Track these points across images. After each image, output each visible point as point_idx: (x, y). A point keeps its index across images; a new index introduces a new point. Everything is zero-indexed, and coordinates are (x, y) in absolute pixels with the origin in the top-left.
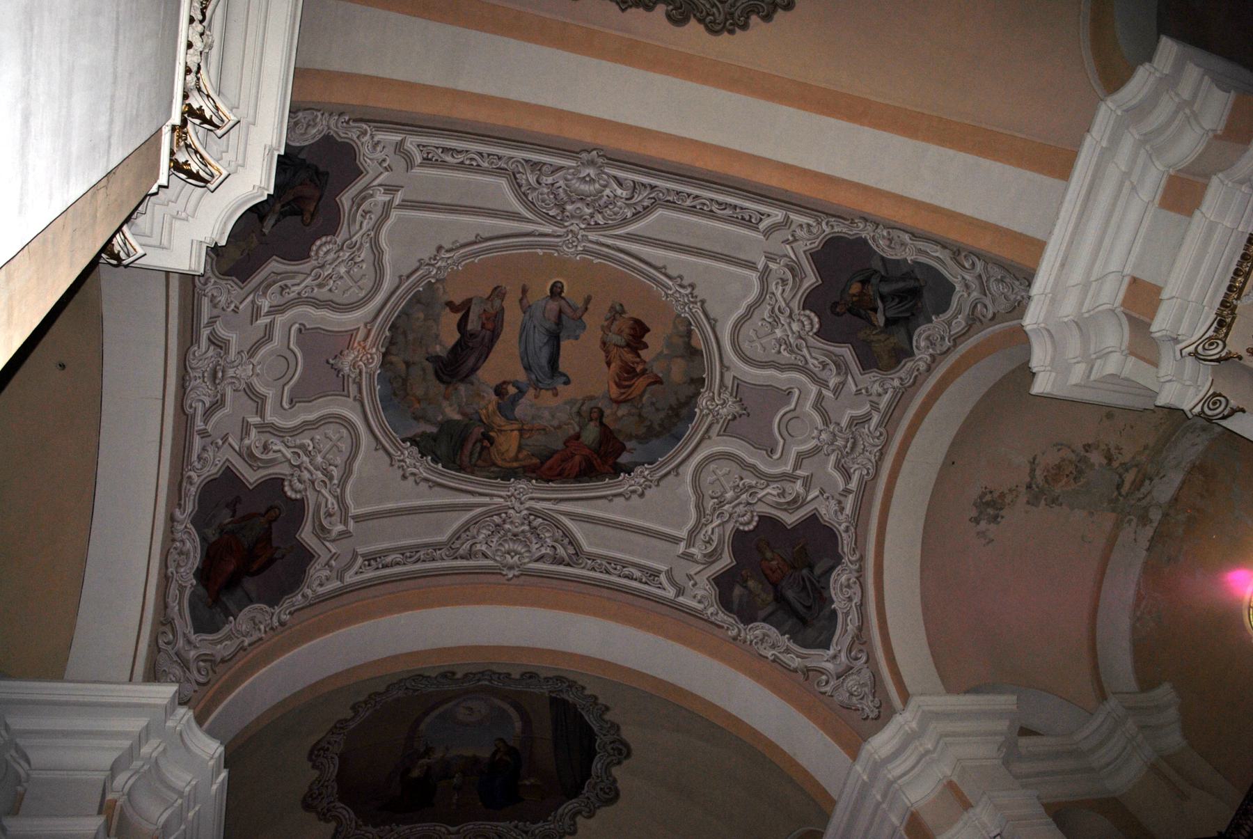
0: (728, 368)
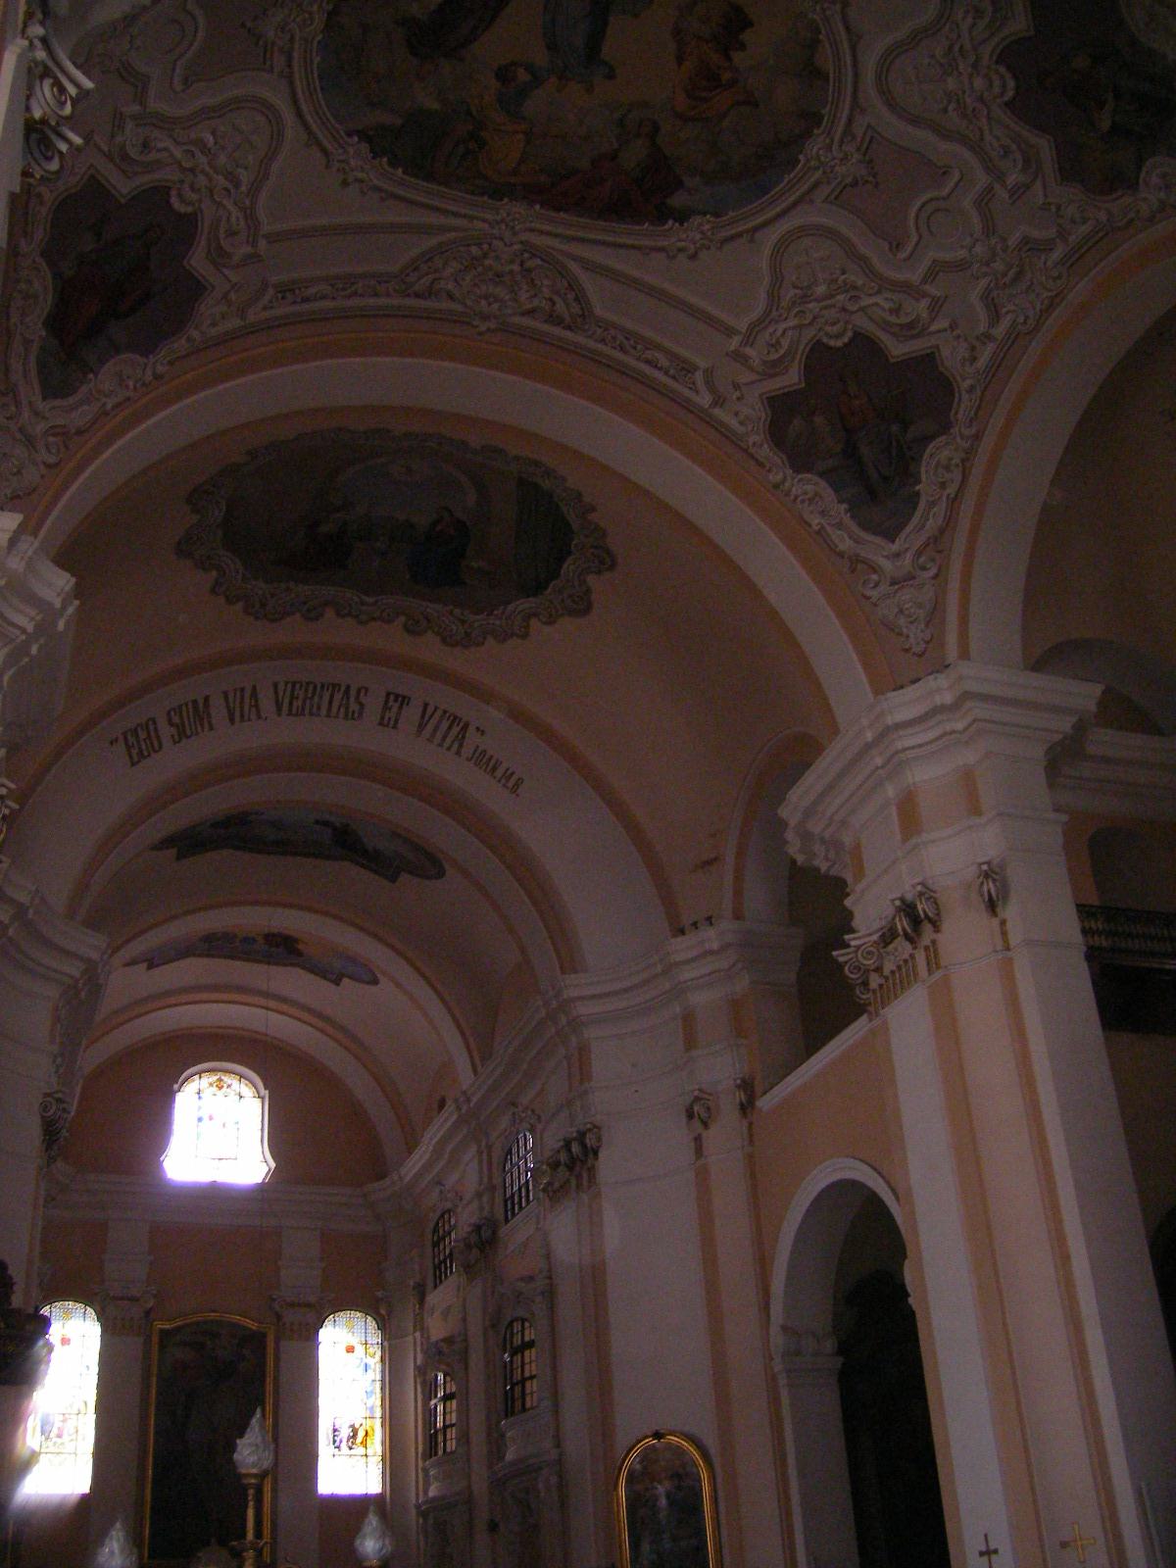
0: (863, 111)
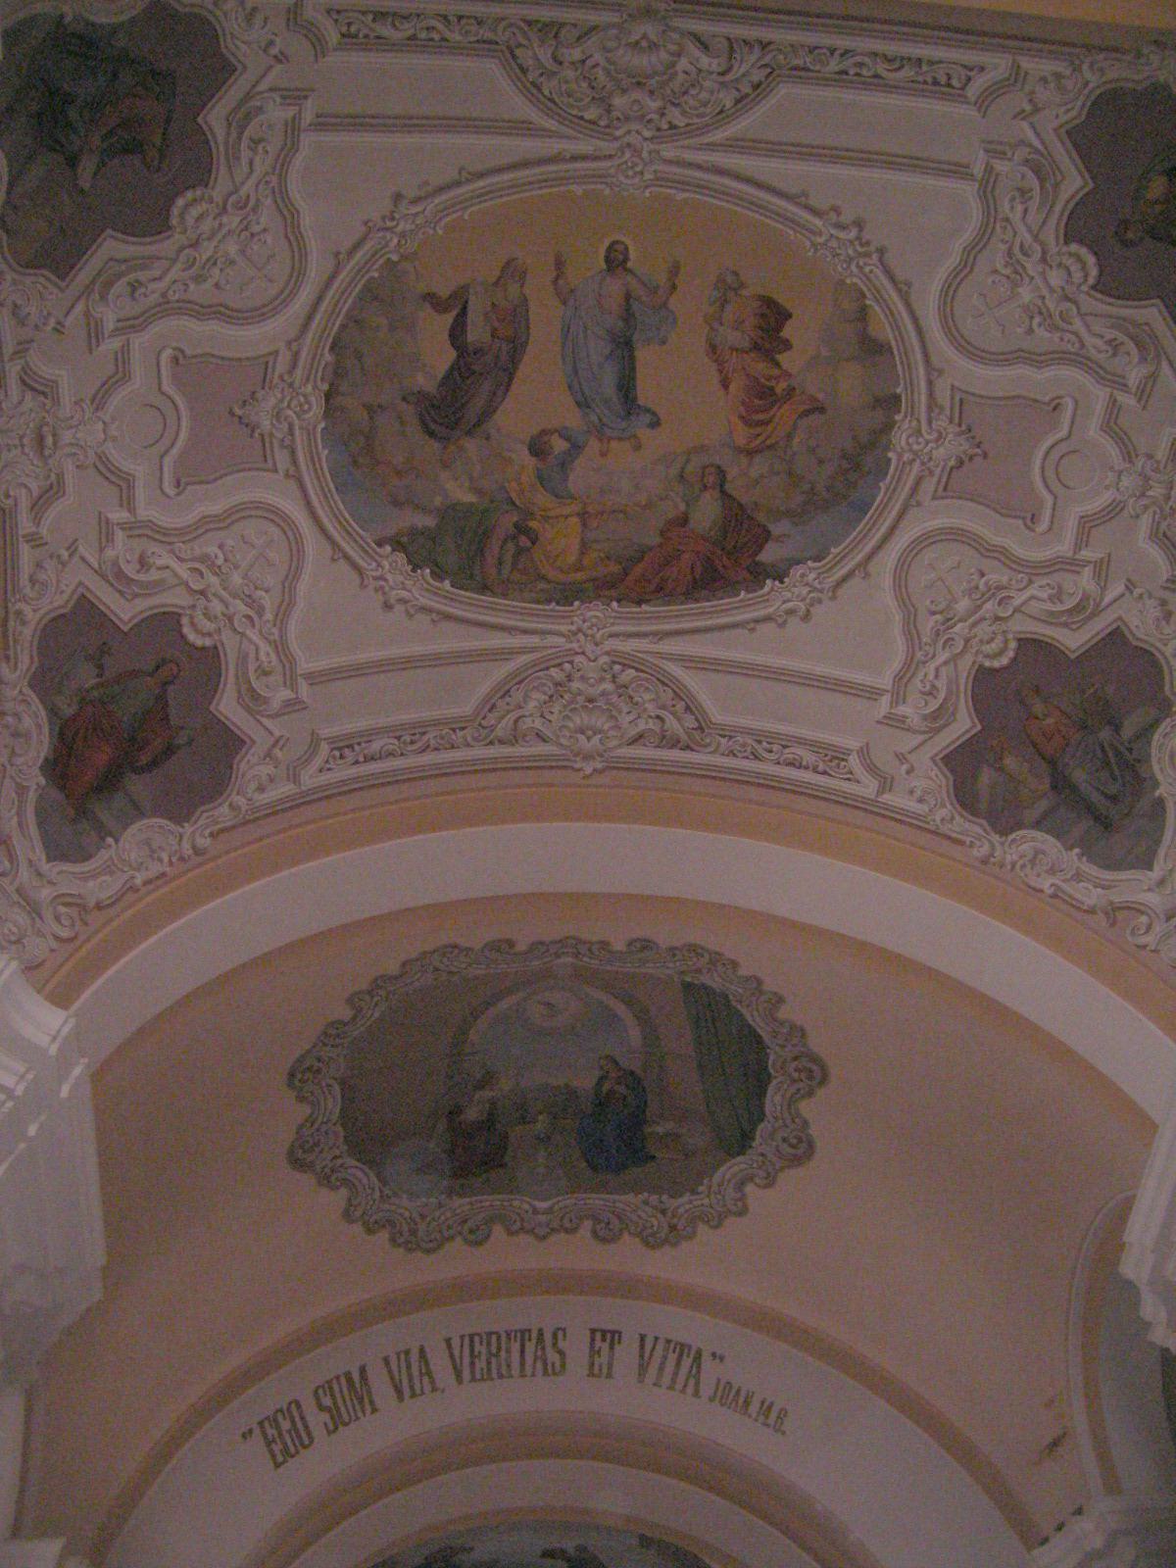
0: (941, 372)
